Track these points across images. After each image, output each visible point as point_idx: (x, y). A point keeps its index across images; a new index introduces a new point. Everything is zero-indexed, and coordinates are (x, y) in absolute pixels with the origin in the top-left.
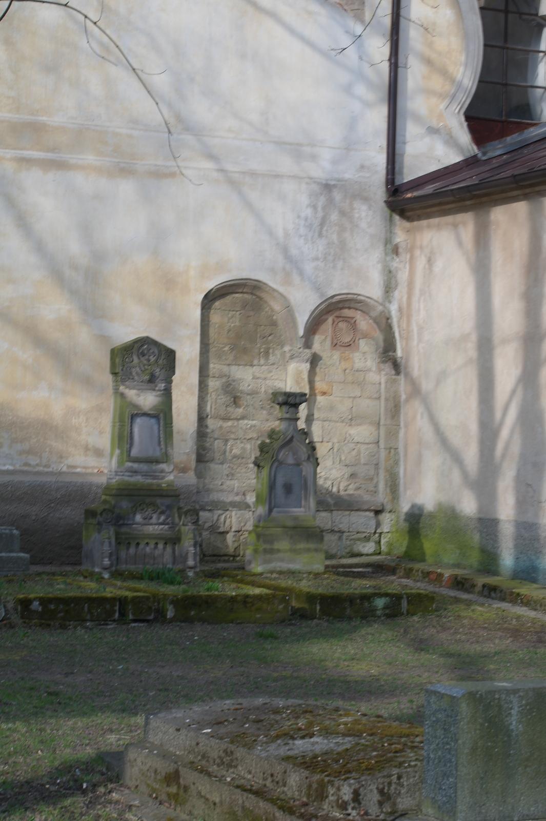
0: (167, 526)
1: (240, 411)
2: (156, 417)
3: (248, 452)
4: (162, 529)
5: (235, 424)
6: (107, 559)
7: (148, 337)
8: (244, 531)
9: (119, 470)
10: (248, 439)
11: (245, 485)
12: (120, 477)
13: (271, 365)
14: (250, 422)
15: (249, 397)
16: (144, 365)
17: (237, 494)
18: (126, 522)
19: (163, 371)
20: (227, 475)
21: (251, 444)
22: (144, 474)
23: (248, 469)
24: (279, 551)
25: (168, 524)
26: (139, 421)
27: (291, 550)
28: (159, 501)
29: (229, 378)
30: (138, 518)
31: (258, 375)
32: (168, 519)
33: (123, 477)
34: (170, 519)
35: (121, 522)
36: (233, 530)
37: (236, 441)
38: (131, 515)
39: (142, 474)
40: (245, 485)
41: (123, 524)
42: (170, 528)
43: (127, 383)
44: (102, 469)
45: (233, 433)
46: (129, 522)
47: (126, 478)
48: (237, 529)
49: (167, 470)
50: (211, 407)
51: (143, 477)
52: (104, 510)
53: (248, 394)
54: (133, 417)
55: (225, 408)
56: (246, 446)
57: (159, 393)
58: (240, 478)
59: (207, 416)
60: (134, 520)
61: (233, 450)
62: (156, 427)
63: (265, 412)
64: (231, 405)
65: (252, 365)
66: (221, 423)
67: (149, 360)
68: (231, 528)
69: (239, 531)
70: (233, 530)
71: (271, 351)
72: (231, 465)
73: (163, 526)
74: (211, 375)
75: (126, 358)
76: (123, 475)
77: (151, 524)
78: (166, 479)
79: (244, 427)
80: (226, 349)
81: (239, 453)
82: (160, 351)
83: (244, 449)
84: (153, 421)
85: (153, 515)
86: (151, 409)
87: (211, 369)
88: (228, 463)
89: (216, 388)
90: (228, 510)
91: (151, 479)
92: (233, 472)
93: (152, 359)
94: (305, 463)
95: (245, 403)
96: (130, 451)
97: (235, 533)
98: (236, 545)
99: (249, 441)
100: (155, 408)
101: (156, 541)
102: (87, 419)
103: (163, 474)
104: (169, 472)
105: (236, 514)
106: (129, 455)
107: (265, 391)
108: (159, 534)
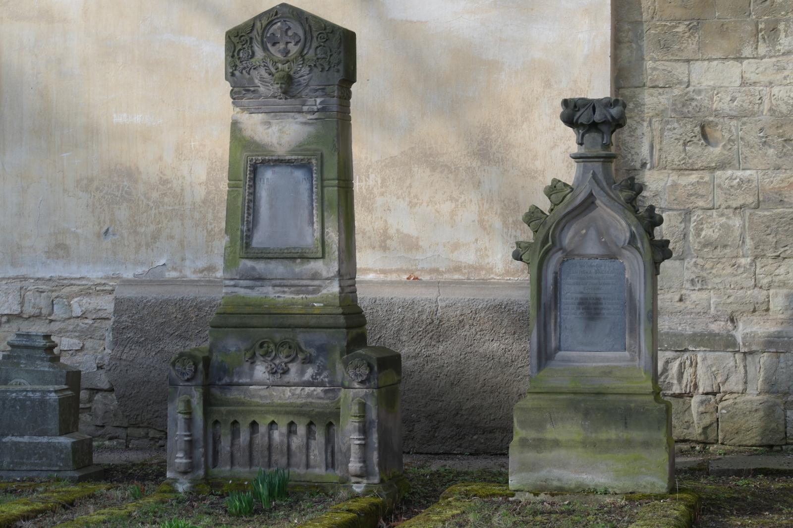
0: (319, 389)
1: (716, 151)
2: (304, 166)
3: (737, 233)
4: (309, 395)
5: (707, 179)
6: (180, 455)
7: (283, 5)
8: (725, 393)
9: (228, 276)
10: (736, 209)
11: (731, 299)
12: (230, 290)
13: (784, 54)
14: (739, 173)
15: (734, 122)
16: (275, 63)
17: (716, 319)
18: (235, 380)
19: (317, 71)
20: (692, 280)
21: (743, 218)
22: (278, 282)
23: (739, 267)
24: (556, 444)
25: (322, 384)
26: (269, 176)
27: (584, 444)
28: (301, 337)
29: (688, 86)
30: (261, 371)
31: (753, 77)
32: (320, 374)
33: (236, 289)
34: (325, 373)
35: (226, 380)
36: (701, 390)
37: (709, 213)
38: (247, 366)
39: (274, 282)
40: (731, 299)
41: (231, 384)
42: (326, 392)
43: (245, 101)
44: (417, 274)
45: (703, 196)
46: (243, 380)
47: (242, 292)
48: (709, 390)
49: (325, 274)
50: (652, 147)
51: (277, 289)
52: (181, 355)
53: (732, 117)
54: (255, 170)
55: (681, 148)
56: (730, 222)
57: (310, 117)
58: (720, 286)
59: (644, 165)
60: (251, 376)
61: (702, 230)
62: (304, 187)
63: (771, 151)
64: (695, 140)
65: (739, 59)
66: (674, 177)
67: (286, 52)
68: (696, 386)
69: (714, 394)
70: (701, 390)
71: (781, 27)
72: (700, 261)
73: (312, 388)
74: (648, 84)
75: (240, 50)
76: (235, 286)
77: (288, 385)
78: (324, 291)
79: (726, 186)
80: (681, 28)
81: (715, 236)
82: (308, 33)
83: (726, 228)
84: (299, 174)
85: (290, 365)
86: (292, 152)
87: (649, 71)
88: (692, 258)
89: (661, 107)
90: (686, 350)
91: (291, 293)
92: (704, 274)
93: (294, 49)
94: (626, 253)
95: (727, 136)
96: (249, 237)
97: (704, 397)
98: (707, 420)
99: (738, 211)
100: (300, 148)
101: (291, 419)
102: (384, 180)
103: (317, 283)
104: (327, 279)
105: (704, 359)
106: (248, 245)
107: (770, 110)
108: (303, 405)
